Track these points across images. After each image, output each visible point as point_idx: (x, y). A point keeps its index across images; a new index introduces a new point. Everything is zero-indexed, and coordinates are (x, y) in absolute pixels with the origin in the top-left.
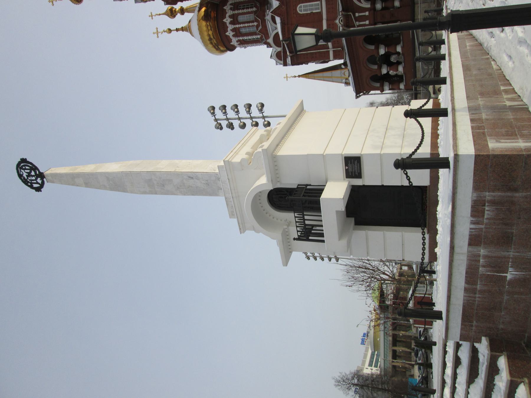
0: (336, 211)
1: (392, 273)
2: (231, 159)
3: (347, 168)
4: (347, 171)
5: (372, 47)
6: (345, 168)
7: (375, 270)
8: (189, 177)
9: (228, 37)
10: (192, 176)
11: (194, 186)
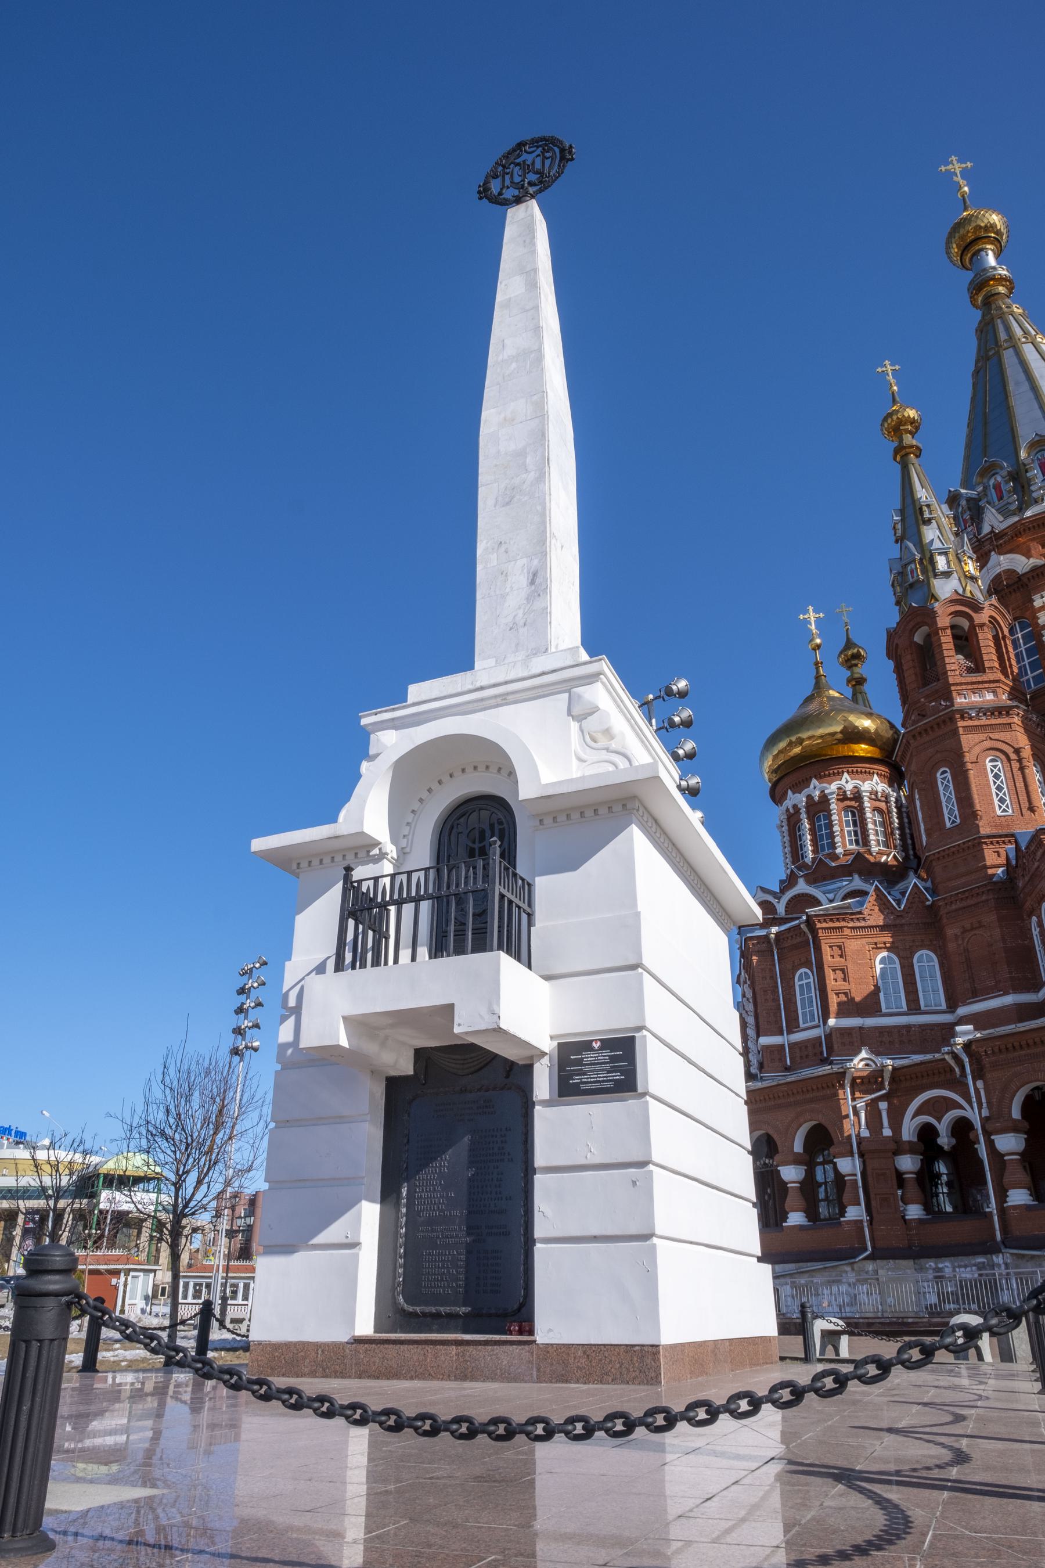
0: (453, 1004)
1: (200, 1208)
2: (605, 680)
3: (596, 1045)
4: (587, 1046)
5: (798, 1147)
6: (596, 1040)
7: (211, 1155)
8: (535, 575)
9: (806, 783)
10: (537, 581)
11: (508, 590)
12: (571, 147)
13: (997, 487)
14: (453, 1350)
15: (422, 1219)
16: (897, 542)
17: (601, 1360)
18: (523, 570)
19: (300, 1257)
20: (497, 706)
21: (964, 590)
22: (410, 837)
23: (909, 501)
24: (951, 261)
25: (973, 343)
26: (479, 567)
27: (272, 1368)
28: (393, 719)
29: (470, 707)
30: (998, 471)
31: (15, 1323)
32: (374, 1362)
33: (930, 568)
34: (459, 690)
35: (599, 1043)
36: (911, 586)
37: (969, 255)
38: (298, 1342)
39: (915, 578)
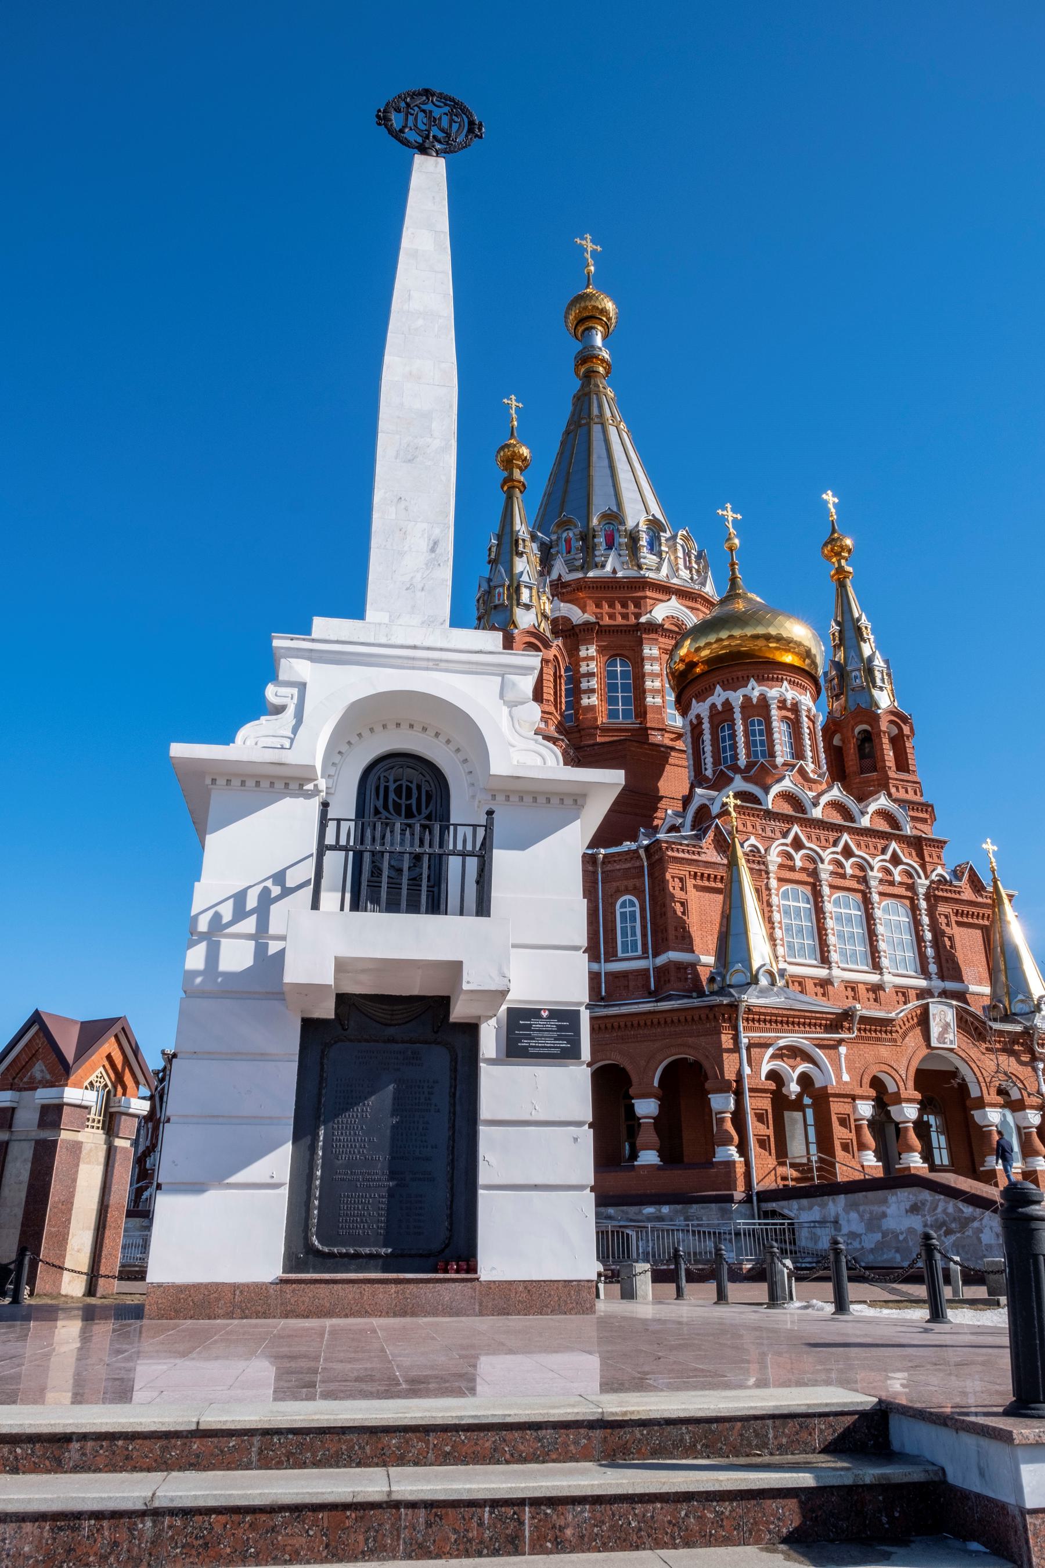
3: (545, 1014)
4: (535, 1013)
8: (435, 543)
9: (710, 691)
12: (480, 125)
13: (568, 541)
14: (393, 1288)
15: (340, 1162)
16: (489, 562)
17: (541, 1294)
18: (423, 535)
19: (213, 1196)
20: (427, 669)
21: (539, 625)
22: (336, 778)
23: (507, 529)
24: (567, 326)
25: (569, 408)
26: (376, 515)
27: (176, 1311)
28: (311, 650)
29: (399, 662)
30: (572, 528)
31: (1010, 1256)
32: (303, 1302)
33: (515, 597)
34: (372, 640)
35: (547, 1013)
36: (496, 607)
37: (583, 328)
38: (209, 1283)
39: (501, 601)
